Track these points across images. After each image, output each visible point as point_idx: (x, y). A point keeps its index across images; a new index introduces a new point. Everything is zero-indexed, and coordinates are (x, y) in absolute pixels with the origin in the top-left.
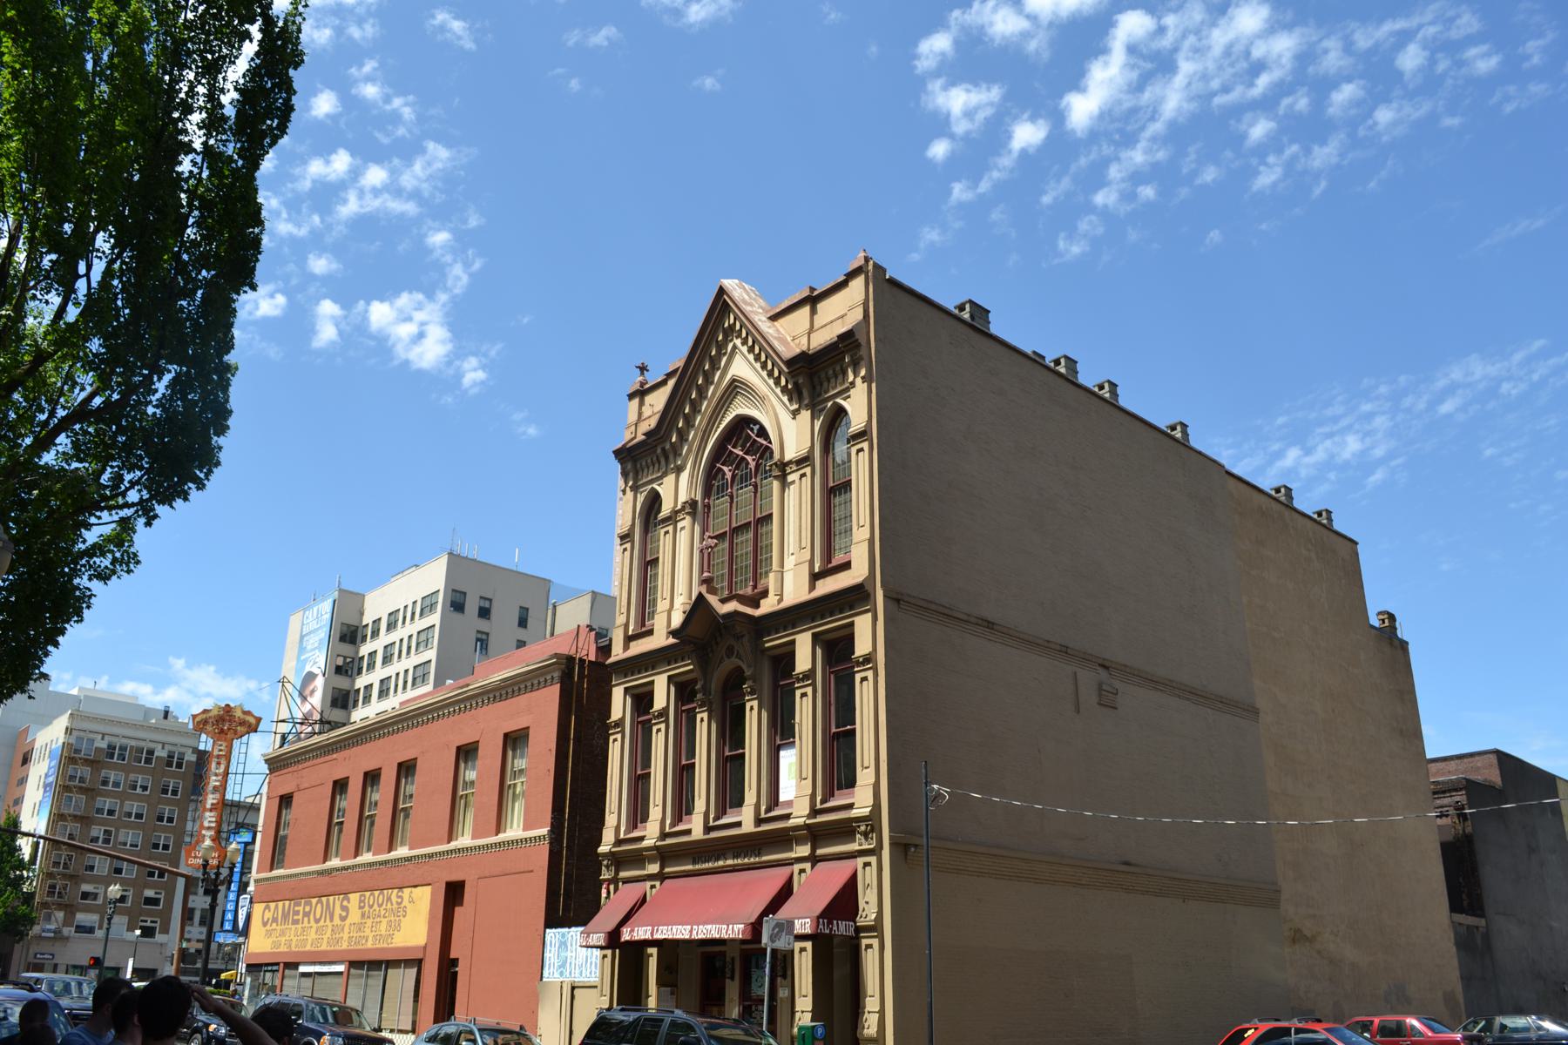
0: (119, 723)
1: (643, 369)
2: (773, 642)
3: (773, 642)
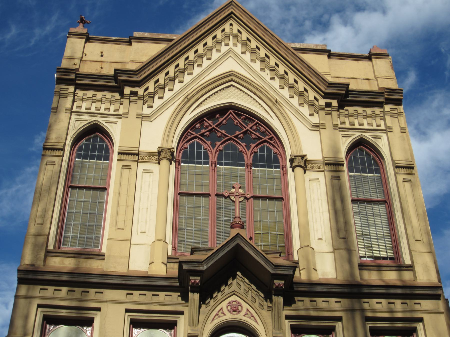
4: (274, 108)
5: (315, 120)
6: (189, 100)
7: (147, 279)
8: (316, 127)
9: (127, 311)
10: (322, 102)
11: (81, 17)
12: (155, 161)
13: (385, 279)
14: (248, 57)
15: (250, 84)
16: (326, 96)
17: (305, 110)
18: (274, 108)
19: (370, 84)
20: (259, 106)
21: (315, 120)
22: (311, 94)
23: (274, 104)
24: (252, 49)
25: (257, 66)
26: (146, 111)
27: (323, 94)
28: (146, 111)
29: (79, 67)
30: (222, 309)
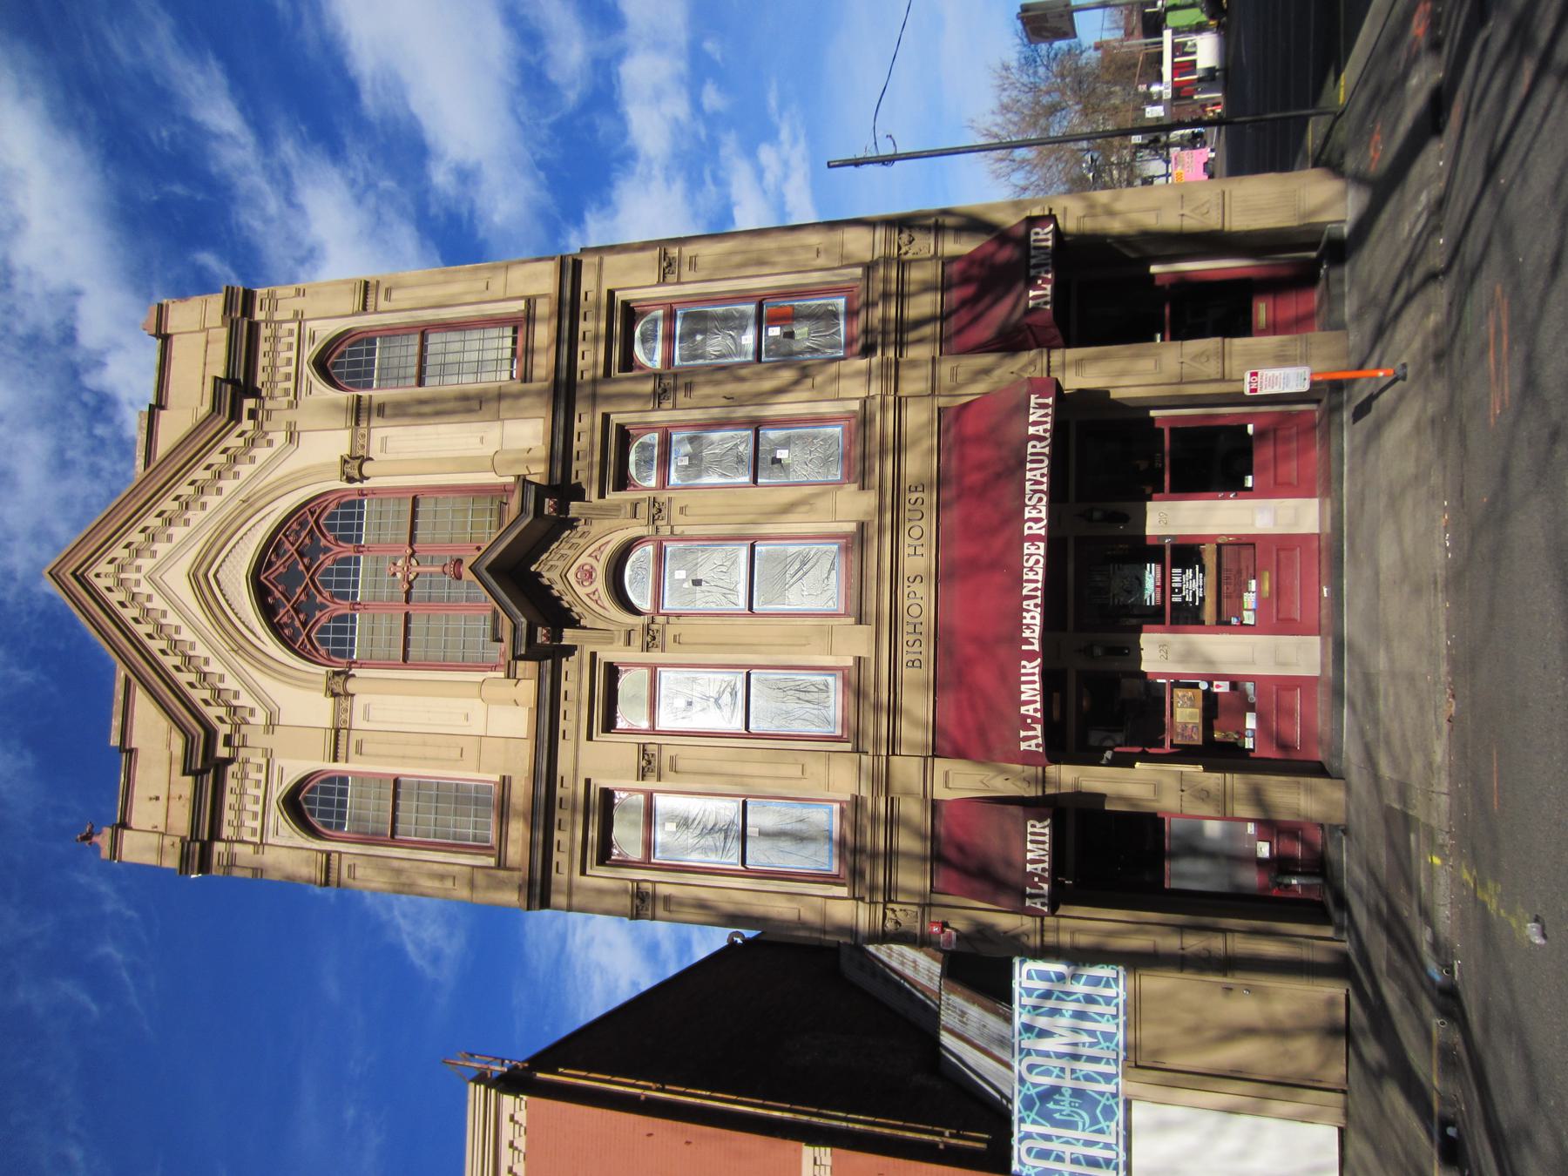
4: (258, 506)
6: (241, 647)
8: (292, 437)
9: (590, 738)
10: (247, 424)
14: (161, 548)
15: (213, 544)
18: (258, 506)
21: (279, 438)
22: (233, 441)
23: (251, 505)
25: (178, 532)
26: (260, 718)
28: (260, 718)
30: (587, 595)
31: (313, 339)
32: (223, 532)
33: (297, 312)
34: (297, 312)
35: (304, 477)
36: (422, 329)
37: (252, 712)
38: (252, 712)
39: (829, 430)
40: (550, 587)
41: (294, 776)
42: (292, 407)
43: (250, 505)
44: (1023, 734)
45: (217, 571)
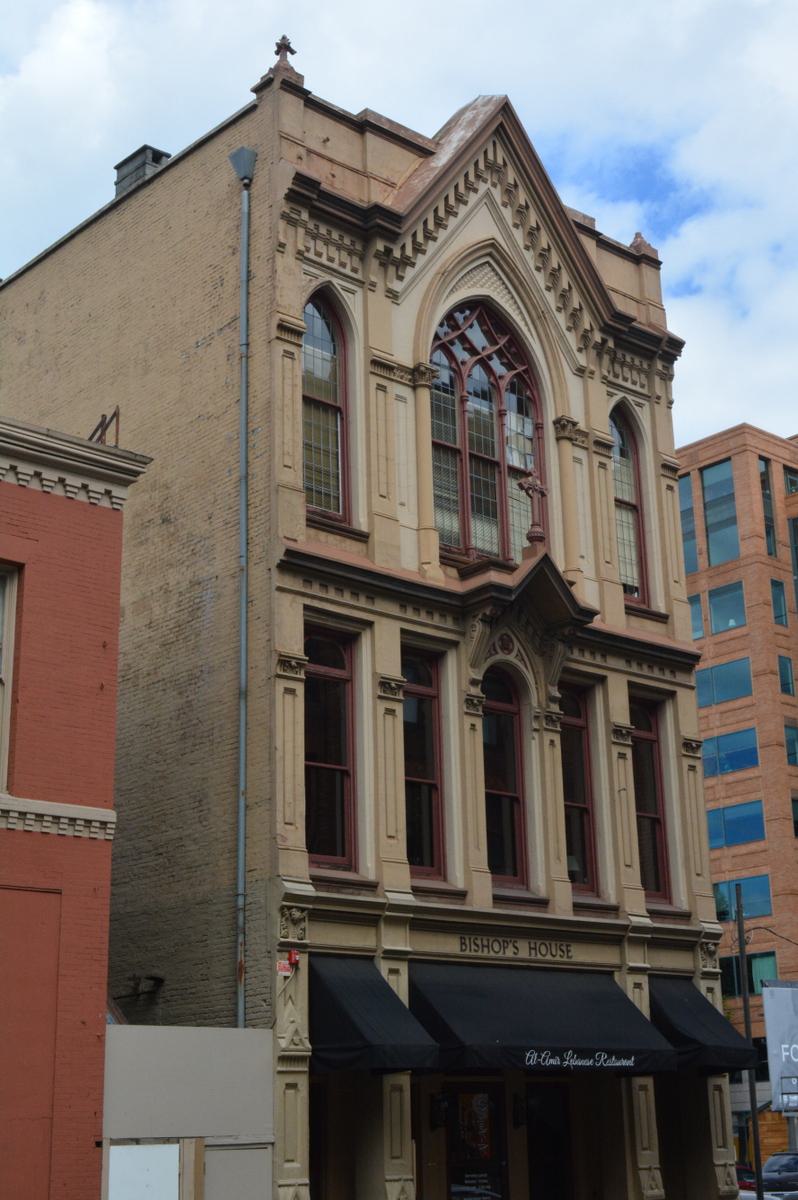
0: (345, 949)
1: (284, 47)
2: (586, 662)
3: (586, 662)
4: (538, 323)
5: (582, 360)
7: (351, 283)
8: (581, 371)
10: (597, 337)
11: (172, 530)
12: (407, 382)
13: (665, 713)
14: (508, 214)
15: (513, 270)
16: (606, 329)
17: (572, 339)
18: (538, 323)
19: (639, 310)
20: (508, 297)
21: (582, 360)
22: (587, 321)
23: (539, 317)
24: (520, 206)
25: (519, 235)
27: (602, 325)
29: (304, 1187)
31: (640, 405)
32: (521, 283)
33: (375, 286)
34: (375, 286)
35: (559, 376)
36: (343, 409)
37: (401, 278)
38: (401, 278)
39: (748, 915)
40: (415, 609)
41: (310, 290)
42: (387, 291)
43: (539, 317)
44: (467, 1176)
45: (490, 265)
